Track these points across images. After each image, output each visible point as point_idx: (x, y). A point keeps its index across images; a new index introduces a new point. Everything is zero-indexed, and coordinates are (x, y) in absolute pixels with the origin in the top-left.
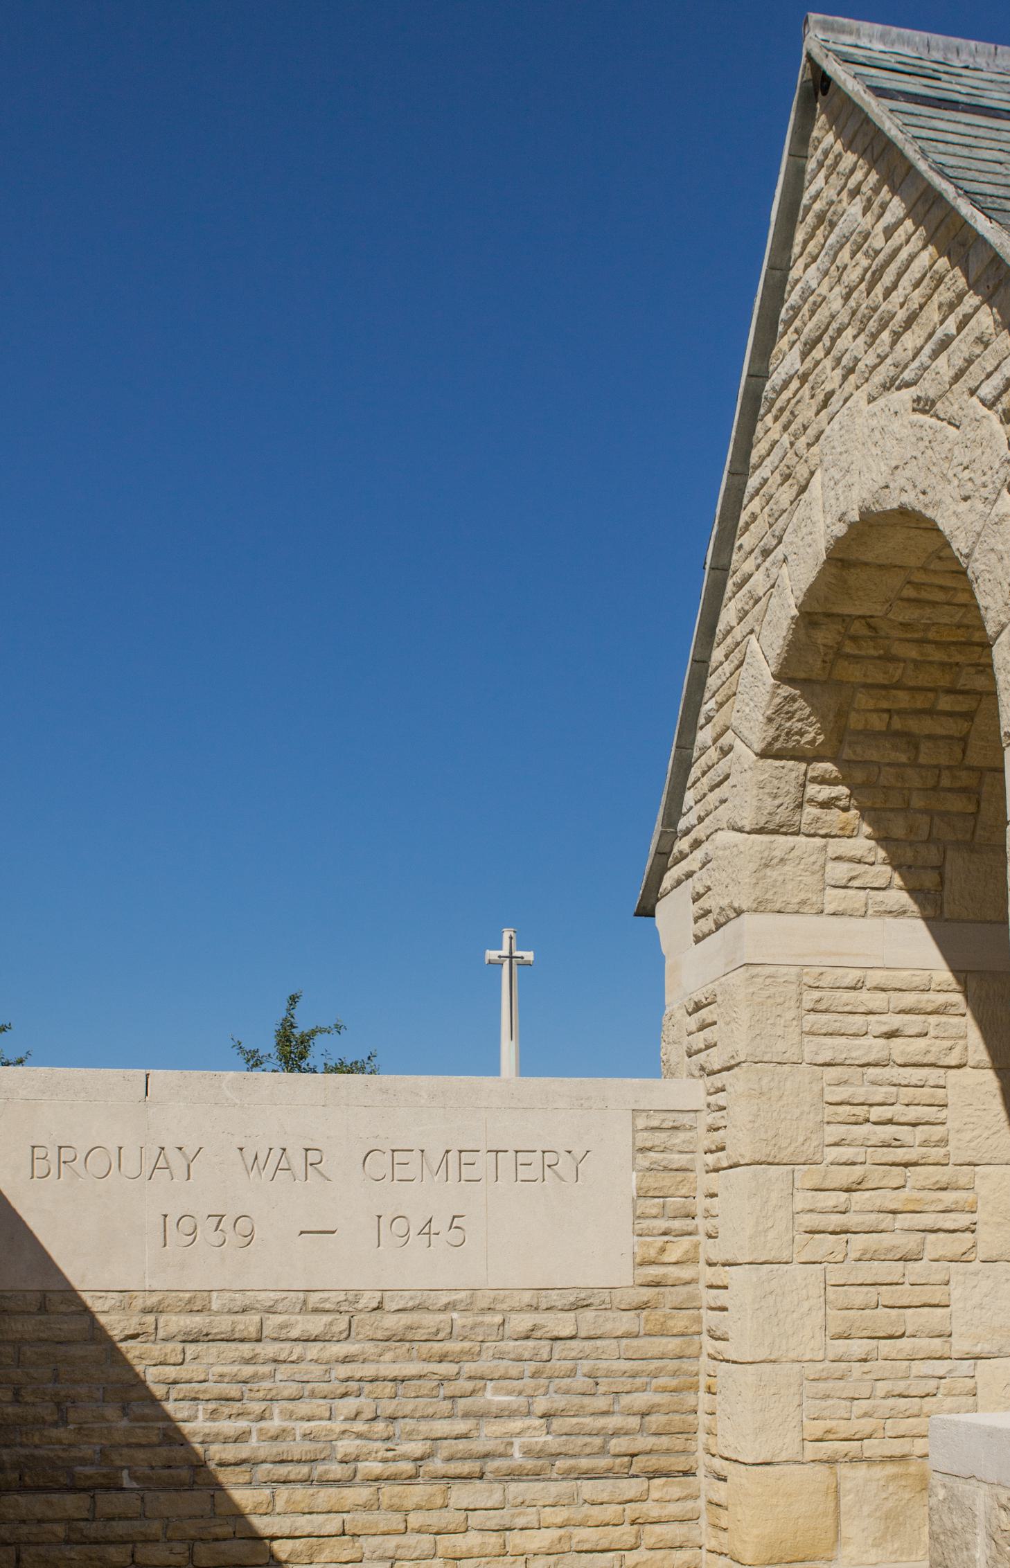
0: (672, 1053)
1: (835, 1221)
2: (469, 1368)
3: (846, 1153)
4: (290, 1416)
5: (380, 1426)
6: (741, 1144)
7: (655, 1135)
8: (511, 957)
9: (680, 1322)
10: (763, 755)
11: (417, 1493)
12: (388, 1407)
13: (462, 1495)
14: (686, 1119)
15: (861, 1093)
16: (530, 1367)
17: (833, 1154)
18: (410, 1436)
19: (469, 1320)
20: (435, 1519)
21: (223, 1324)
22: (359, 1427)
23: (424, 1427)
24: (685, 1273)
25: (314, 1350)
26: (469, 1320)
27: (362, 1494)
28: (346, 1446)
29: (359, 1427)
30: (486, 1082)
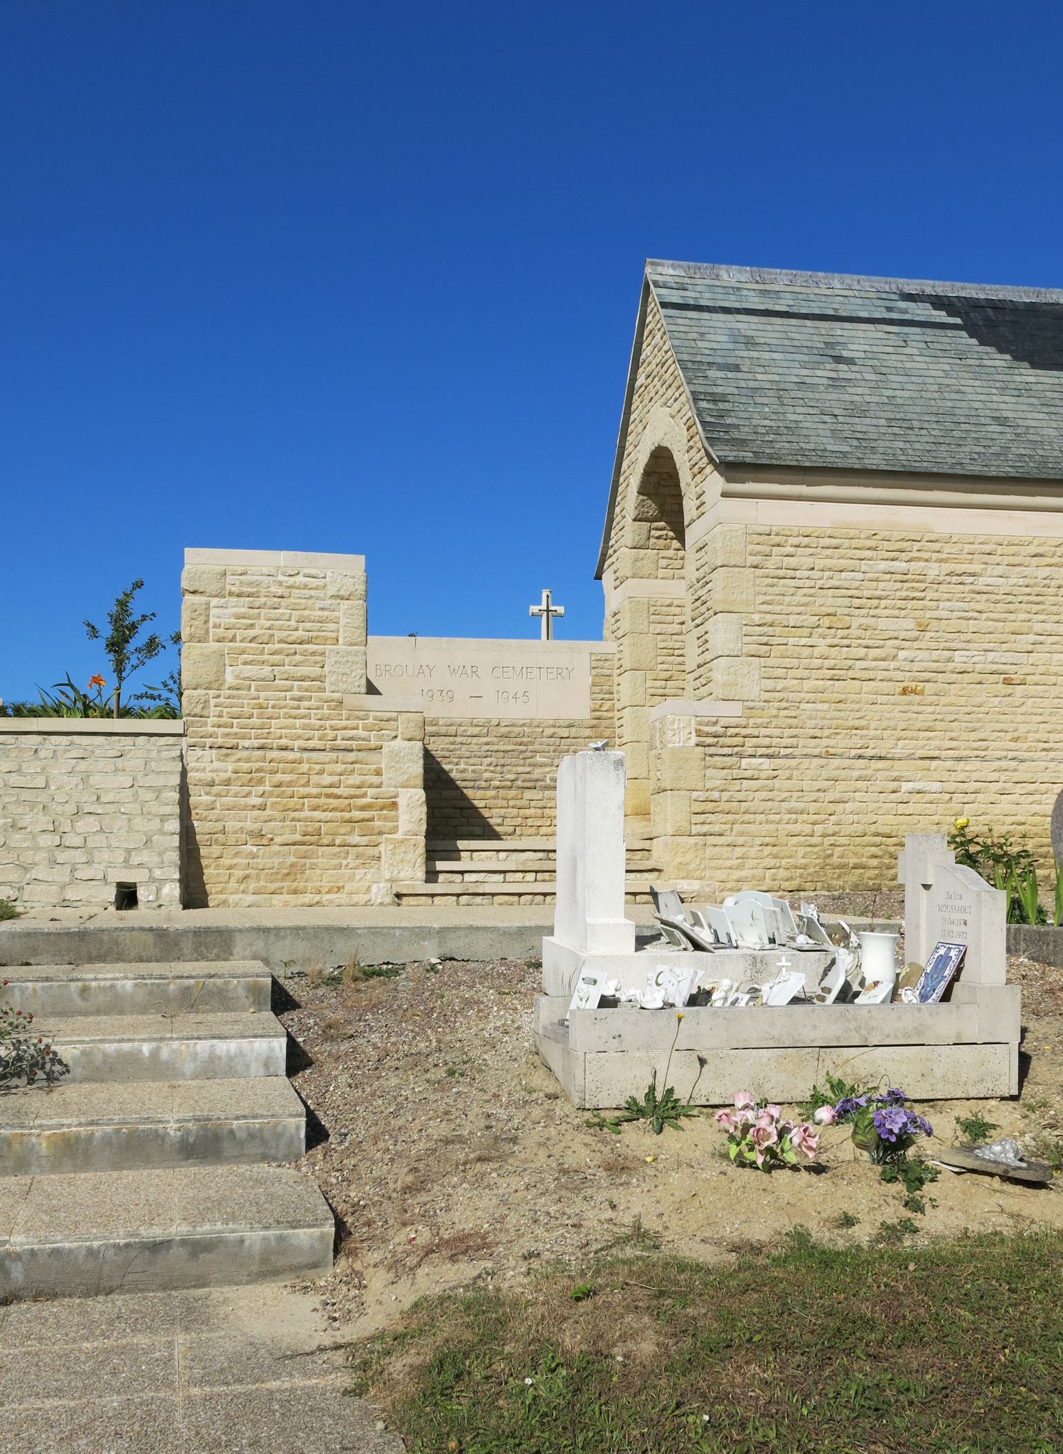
0: (606, 633)
1: (661, 691)
2: (530, 748)
3: (665, 667)
4: (467, 764)
5: (499, 768)
6: (627, 664)
7: (600, 661)
8: (548, 611)
9: (608, 732)
10: (635, 520)
11: (512, 793)
12: (502, 761)
13: (528, 794)
14: (610, 657)
15: (671, 645)
16: (552, 748)
17: (660, 667)
18: (509, 772)
19: (531, 730)
20: (519, 803)
21: (443, 730)
22: (491, 768)
23: (514, 769)
24: (610, 715)
25: (475, 740)
26: (531, 730)
27: (493, 793)
28: (487, 775)
29: (491, 768)
30: (536, 641)
